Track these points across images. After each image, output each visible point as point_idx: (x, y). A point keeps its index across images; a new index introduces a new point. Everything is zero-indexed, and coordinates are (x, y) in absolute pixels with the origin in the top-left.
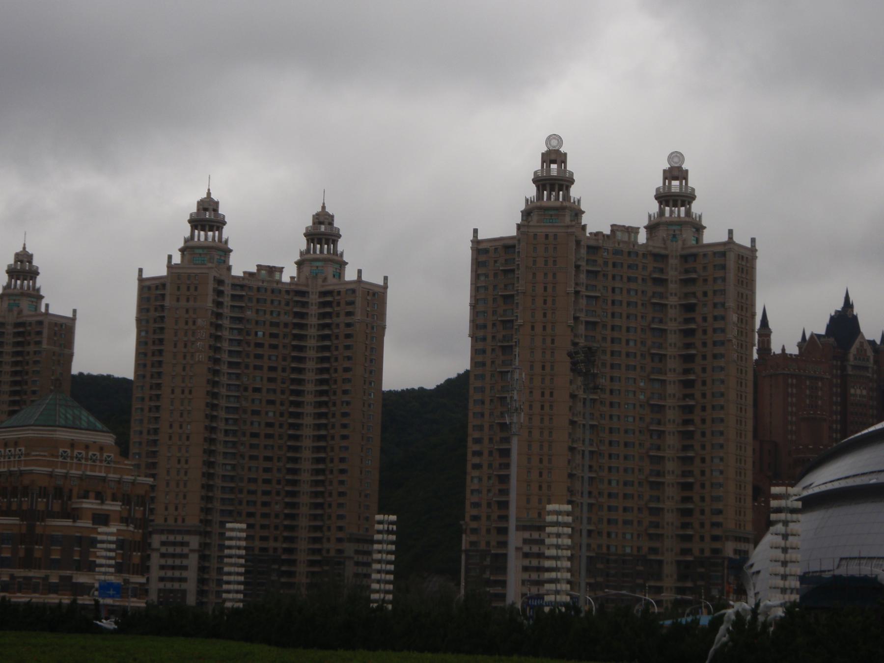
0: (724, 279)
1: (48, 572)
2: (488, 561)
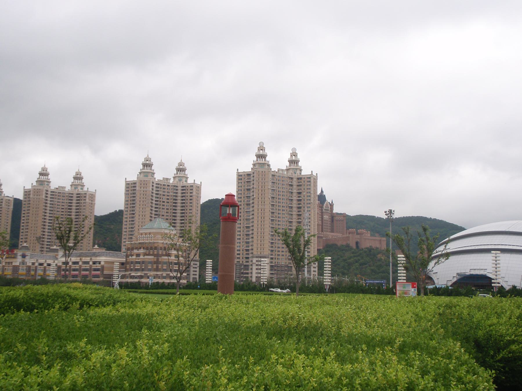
0: (310, 185)
2: (243, 267)
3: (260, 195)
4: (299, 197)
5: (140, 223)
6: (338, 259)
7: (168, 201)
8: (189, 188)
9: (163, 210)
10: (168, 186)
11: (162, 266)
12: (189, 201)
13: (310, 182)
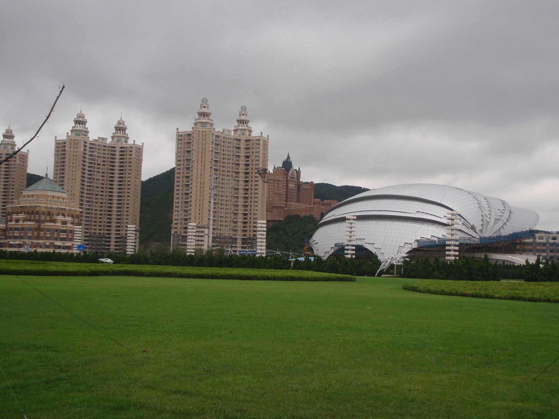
0: (259, 148)
1: (46, 241)
3: (200, 158)
4: (247, 161)
5: (70, 187)
6: (299, 231)
7: (104, 163)
8: (128, 150)
9: (98, 174)
10: (105, 146)
11: (45, 234)
12: (128, 164)
13: (259, 144)
